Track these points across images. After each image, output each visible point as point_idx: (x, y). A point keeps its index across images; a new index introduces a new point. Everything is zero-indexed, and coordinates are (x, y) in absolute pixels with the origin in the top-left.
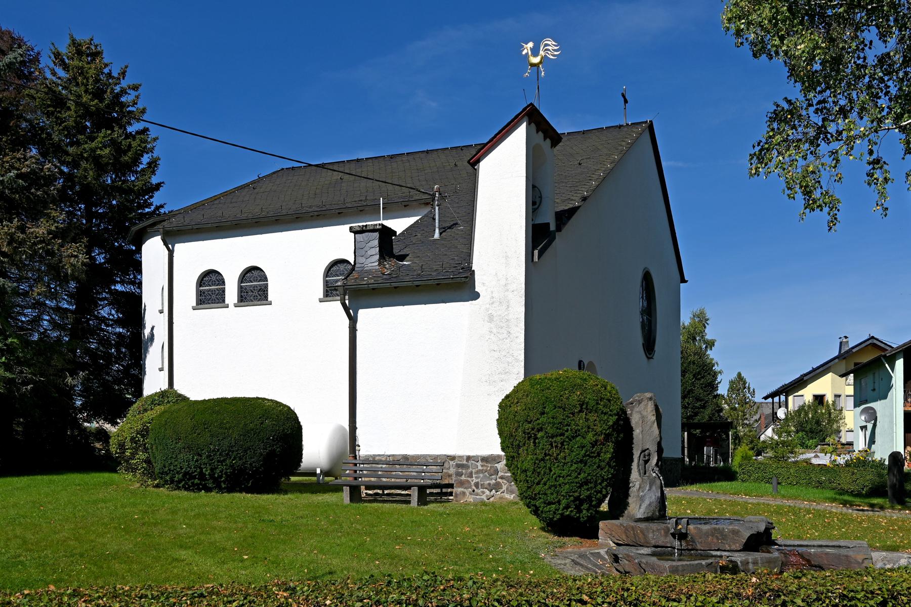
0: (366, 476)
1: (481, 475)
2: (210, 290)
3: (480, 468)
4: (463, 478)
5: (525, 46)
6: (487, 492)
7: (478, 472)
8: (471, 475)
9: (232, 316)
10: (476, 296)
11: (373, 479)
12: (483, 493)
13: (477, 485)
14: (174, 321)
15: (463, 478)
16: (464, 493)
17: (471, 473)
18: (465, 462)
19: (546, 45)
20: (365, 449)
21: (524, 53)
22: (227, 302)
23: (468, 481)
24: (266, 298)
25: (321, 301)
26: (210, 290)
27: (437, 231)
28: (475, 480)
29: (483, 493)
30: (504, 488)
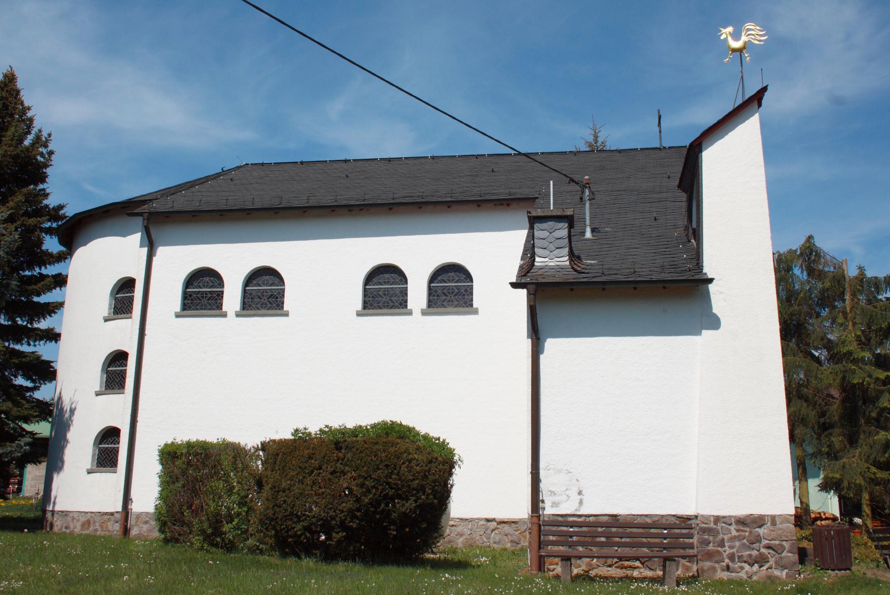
0: (553, 543)
1: (737, 544)
2: (202, 292)
3: (734, 533)
4: (711, 547)
5: (723, 31)
6: (747, 567)
7: (732, 539)
8: (722, 544)
9: (232, 329)
10: (714, 323)
11: (561, 548)
12: (742, 568)
13: (732, 557)
14: (147, 332)
15: (711, 547)
16: (714, 569)
17: (723, 540)
18: (712, 525)
19: (749, 30)
20: (549, 510)
21: (722, 37)
22: (225, 308)
23: (718, 551)
24: (220, 307)
25: (178, 316)
26: (202, 292)
27: (588, 230)
28: (729, 551)
29: (742, 568)
30: (772, 562)
